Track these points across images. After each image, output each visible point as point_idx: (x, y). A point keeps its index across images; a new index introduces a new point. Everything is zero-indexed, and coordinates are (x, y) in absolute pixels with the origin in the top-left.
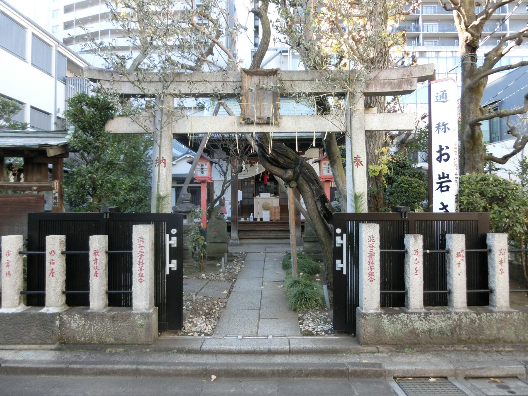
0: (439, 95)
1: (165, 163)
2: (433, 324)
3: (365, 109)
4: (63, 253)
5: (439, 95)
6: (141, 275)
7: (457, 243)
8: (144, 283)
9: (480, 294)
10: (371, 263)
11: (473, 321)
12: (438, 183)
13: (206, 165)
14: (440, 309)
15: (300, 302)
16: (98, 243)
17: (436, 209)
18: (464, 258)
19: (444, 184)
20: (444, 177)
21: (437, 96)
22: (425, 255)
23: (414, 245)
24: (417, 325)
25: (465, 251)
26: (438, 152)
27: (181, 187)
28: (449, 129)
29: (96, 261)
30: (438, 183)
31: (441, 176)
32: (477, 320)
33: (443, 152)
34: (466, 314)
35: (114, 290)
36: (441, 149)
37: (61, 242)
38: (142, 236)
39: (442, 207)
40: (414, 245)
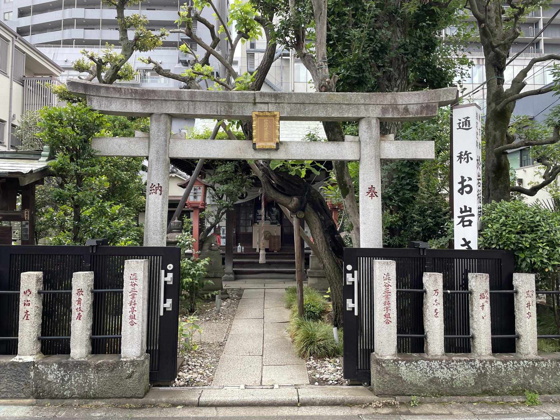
0: (461, 122)
1: (161, 190)
2: (455, 372)
3: (381, 136)
4: (39, 293)
5: (461, 122)
6: (133, 317)
7: (479, 284)
8: (135, 326)
9: (505, 339)
10: (387, 303)
11: (498, 370)
12: (459, 217)
13: (200, 189)
14: (463, 357)
15: (312, 349)
16: (82, 282)
17: (458, 246)
18: (489, 300)
19: (466, 219)
20: (466, 211)
21: (460, 123)
22: (445, 295)
23: (433, 283)
24: (438, 374)
25: (489, 291)
26: (459, 183)
27: (174, 211)
28: (472, 159)
29: (79, 301)
30: (459, 217)
31: (463, 210)
32: (503, 368)
33: (465, 184)
34: (491, 362)
35: (99, 289)
36: (463, 180)
37: (38, 280)
38: (135, 272)
39: (464, 243)
40: (433, 283)
